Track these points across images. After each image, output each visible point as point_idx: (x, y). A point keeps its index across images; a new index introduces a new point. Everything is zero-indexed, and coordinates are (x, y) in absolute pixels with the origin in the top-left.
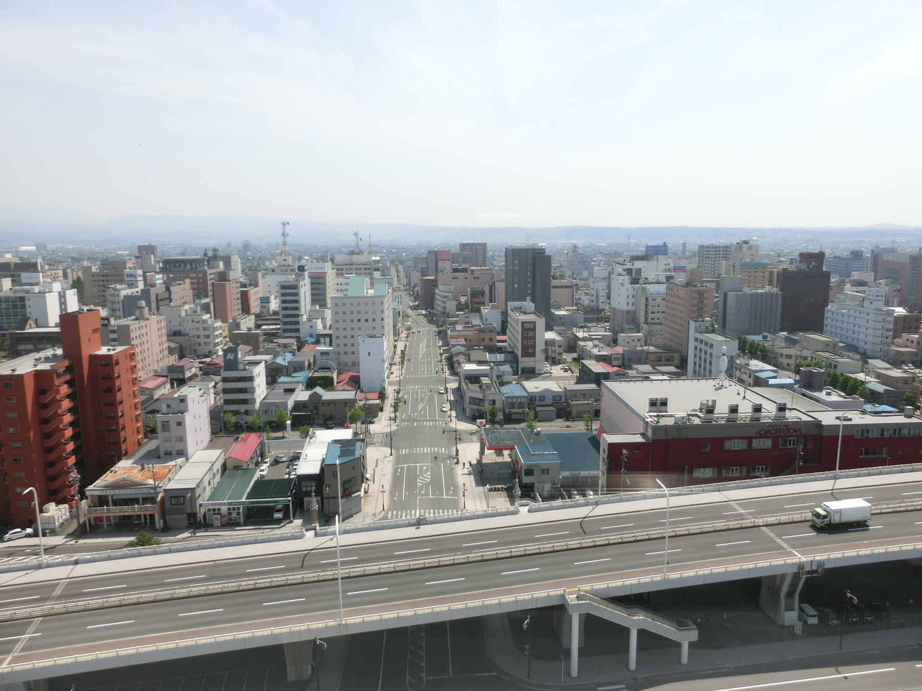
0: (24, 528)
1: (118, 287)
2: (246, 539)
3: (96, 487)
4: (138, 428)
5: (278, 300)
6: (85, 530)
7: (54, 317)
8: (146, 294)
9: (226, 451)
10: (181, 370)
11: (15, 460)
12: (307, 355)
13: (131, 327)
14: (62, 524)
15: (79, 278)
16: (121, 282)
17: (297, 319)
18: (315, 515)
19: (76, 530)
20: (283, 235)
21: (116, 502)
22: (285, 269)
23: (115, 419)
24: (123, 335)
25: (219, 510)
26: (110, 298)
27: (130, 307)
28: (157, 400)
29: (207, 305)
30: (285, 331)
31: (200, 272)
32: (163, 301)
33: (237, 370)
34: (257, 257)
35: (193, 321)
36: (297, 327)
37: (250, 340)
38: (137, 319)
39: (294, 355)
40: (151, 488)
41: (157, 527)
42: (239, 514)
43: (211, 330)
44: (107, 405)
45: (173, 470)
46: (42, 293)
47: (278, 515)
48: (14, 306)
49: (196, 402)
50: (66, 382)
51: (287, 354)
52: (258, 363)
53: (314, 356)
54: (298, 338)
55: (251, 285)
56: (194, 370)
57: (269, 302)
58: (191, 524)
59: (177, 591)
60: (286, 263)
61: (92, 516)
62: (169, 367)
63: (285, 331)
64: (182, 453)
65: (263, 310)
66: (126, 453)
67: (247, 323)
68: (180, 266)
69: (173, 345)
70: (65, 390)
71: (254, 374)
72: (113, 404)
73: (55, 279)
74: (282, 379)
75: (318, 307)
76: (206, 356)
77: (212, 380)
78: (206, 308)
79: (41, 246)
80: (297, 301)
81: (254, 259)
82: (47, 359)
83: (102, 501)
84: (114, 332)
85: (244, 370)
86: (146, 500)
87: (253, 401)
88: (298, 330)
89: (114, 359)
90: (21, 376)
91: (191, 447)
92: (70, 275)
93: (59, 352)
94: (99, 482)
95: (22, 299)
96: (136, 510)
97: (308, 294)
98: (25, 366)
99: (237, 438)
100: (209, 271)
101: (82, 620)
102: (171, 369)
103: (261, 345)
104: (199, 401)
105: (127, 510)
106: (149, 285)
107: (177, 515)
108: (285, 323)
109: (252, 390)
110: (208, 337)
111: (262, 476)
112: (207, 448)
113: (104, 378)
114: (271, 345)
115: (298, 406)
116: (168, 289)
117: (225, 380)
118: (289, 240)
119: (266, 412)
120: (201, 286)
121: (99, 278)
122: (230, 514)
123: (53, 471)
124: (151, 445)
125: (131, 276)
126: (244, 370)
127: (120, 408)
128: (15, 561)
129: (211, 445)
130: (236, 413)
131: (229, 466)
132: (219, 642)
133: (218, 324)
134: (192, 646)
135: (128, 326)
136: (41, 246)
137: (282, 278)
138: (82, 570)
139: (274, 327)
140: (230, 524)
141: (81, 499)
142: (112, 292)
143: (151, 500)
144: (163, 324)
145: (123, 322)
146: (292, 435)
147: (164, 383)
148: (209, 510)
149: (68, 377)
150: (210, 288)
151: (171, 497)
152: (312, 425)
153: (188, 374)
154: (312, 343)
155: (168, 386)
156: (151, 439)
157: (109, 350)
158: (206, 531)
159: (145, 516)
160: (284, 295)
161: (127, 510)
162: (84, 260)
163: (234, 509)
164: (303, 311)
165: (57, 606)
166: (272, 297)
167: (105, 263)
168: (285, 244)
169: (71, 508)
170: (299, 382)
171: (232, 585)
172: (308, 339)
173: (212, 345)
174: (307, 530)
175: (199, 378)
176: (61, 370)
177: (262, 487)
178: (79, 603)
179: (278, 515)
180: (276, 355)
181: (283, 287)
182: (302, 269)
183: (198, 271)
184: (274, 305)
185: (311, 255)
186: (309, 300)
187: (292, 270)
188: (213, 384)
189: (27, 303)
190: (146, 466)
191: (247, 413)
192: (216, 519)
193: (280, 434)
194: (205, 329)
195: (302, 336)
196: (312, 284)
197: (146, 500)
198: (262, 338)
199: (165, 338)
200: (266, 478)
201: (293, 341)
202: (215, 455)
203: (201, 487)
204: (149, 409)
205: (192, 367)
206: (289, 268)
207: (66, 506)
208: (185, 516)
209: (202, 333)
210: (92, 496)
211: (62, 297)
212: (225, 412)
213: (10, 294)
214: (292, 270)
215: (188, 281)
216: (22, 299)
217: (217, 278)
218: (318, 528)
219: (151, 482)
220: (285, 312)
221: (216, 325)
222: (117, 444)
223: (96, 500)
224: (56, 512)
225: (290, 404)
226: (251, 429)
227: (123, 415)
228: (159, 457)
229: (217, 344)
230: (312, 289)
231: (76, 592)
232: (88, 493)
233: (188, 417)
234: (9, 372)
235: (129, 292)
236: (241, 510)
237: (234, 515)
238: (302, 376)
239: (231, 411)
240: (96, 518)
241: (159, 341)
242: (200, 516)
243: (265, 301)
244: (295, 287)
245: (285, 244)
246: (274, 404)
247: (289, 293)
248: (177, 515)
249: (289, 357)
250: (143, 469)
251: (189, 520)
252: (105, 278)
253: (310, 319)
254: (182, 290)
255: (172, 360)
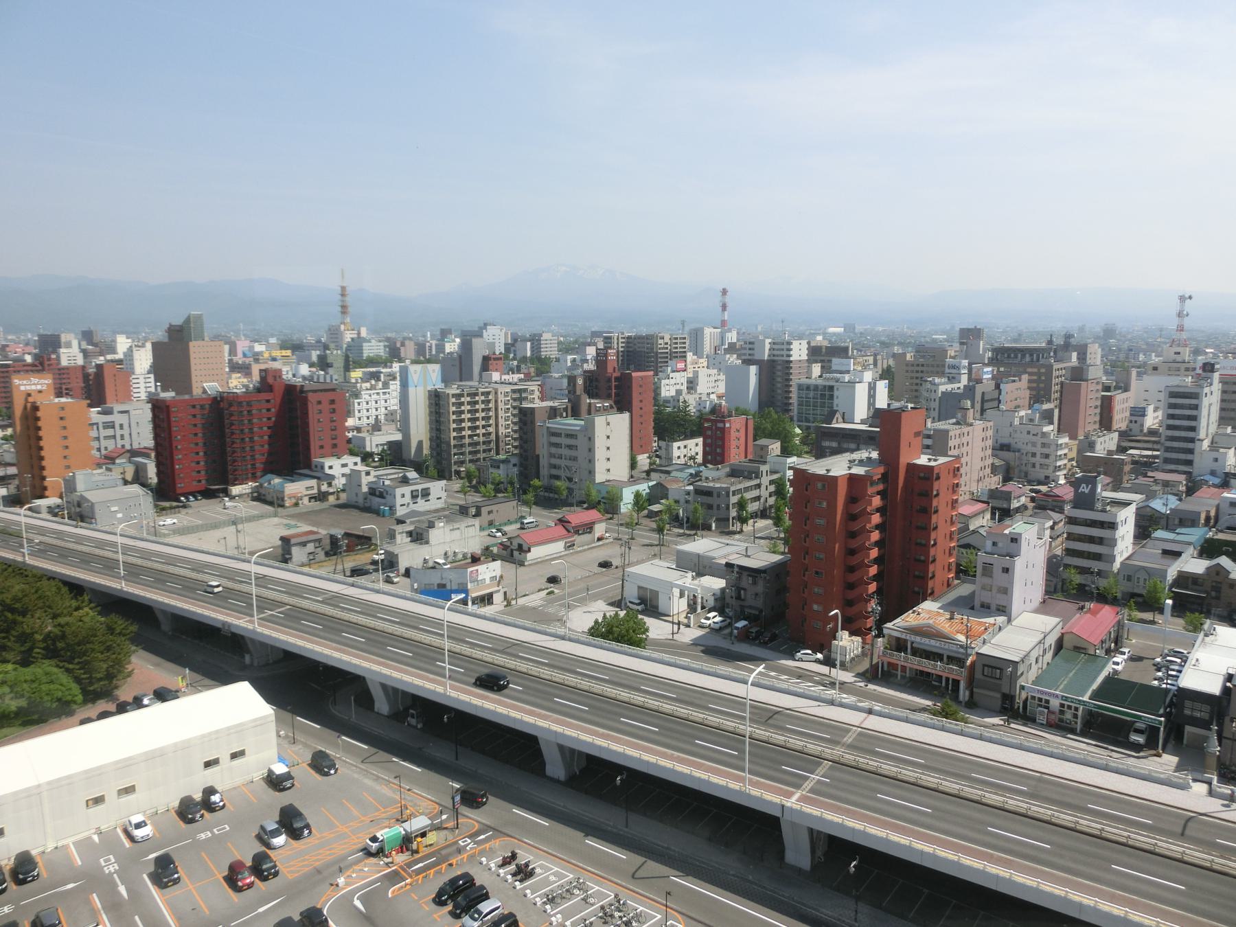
0: (815, 652)
1: (937, 380)
2: (1067, 753)
3: (895, 626)
4: (950, 564)
5: (1160, 414)
6: (879, 674)
7: (861, 411)
8: (969, 391)
9: (1065, 621)
10: (1007, 497)
11: (817, 573)
12: (1206, 501)
13: (951, 433)
14: (853, 659)
15: (889, 367)
16: (941, 374)
17: (1190, 445)
18: (1213, 762)
19: (866, 671)
20: (1180, 315)
21: (917, 652)
22: (1175, 366)
23: (926, 547)
24: (937, 443)
25: (1047, 702)
26: (925, 394)
27: (951, 407)
28: (974, 532)
29: (1051, 412)
30: (1166, 461)
31: (1043, 366)
32: (989, 404)
33: (1092, 509)
34: (1125, 346)
35: (1029, 433)
36: (1189, 457)
37: (1110, 467)
38: (958, 423)
39: (1180, 500)
40: (961, 646)
41: (961, 698)
42: (1075, 716)
43: (1053, 447)
44: (918, 528)
45: (990, 630)
46: (852, 383)
47: (1140, 739)
48: (823, 396)
49: (1032, 545)
50: (878, 493)
51: (1170, 497)
52: (1126, 504)
53: (1218, 507)
54: (1189, 474)
55: (1117, 388)
56: (1023, 499)
57: (1144, 415)
58: (1005, 709)
59: (987, 795)
60: (1179, 358)
61: (886, 660)
62: (991, 490)
63: (1166, 461)
64: (1003, 610)
65: (1133, 426)
66: (932, 593)
67: (1106, 444)
68: (1016, 357)
69: (998, 462)
70: (877, 501)
71: (1118, 520)
72: (926, 529)
73: (865, 367)
74: (1159, 534)
75: (1229, 430)
76: (1040, 483)
77: (1050, 518)
78: (1047, 417)
79: (849, 328)
80: (1194, 418)
81: (1120, 350)
82: (861, 463)
83: (899, 645)
84: (929, 437)
85: (1104, 511)
86: (951, 659)
87: (1112, 558)
88: (1189, 463)
89: (936, 472)
90: (835, 478)
91: (1016, 605)
92: (879, 363)
93: (875, 455)
94: (898, 621)
95: (831, 388)
96: (936, 668)
97: (1215, 410)
98: (838, 466)
99: (1082, 608)
100: (1055, 367)
101: (873, 784)
102: (993, 494)
103: (1125, 478)
104: (1035, 544)
105: (927, 666)
106: (975, 380)
107: (982, 690)
108: (1168, 449)
109: (1113, 543)
110: (1047, 456)
111: (1115, 672)
112: (1037, 611)
113: (920, 495)
114: (1141, 480)
115: (1184, 579)
116: (998, 387)
117: (1072, 521)
118: (1187, 322)
119: (1129, 578)
120: (1042, 385)
121: (915, 367)
122: (1062, 712)
123: (851, 595)
124: (964, 589)
125: (954, 367)
126: (1104, 511)
127: (933, 535)
128: (805, 686)
129: (1044, 608)
130: (1083, 571)
131: (1066, 643)
132: (962, 865)
133: (1064, 440)
134: (1004, 879)
135: (947, 431)
136: (849, 328)
137: (1174, 381)
138: (874, 723)
139: (1149, 453)
140: (1060, 726)
141: (878, 636)
142: (929, 386)
143: (960, 662)
144: (990, 433)
145: (941, 425)
146: (1170, 624)
147: (983, 512)
148: (1033, 698)
149: (881, 487)
150: (1056, 388)
151: (984, 665)
152: (1208, 614)
153: (1015, 504)
154: (1215, 486)
155: (988, 516)
156: (963, 582)
157: (930, 460)
158: (1025, 725)
159: (947, 679)
160: (1172, 406)
161: (927, 666)
162: (894, 345)
163: (1069, 707)
164: (1202, 435)
165: (847, 756)
166: (1150, 409)
167: (921, 350)
168: (1181, 329)
169: (864, 642)
170: (1189, 544)
171: (1066, 818)
172: (1207, 477)
173: (1051, 469)
174: (1195, 780)
175: (1030, 512)
176: (876, 478)
177: (1114, 688)
178: (871, 763)
179: (1140, 739)
180: (1151, 495)
181: (1173, 395)
182: (1209, 368)
183: (1039, 366)
184: (1152, 419)
185: (1217, 347)
186: (1215, 416)
187: (1187, 369)
188: (1051, 523)
189: (836, 393)
190: (957, 616)
191: (1100, 573)
192: (1041, 713)
193: (1148, 616)
194: (1044, 445)
195: (1194, 474)
196: (1224, 392)
197: (951, 659)
198: (1127, 468)
199: (989, 452)
200: (1122, 677)
201: (1182, 478)
202: (1049, 624)
203: (1027, 663)
204: (962, 542)
205: (1021, 497)
206: (1183, 366)
207: (859, 639)
208: (998, 696)
209: (1039, 450)
210: (890, 636)
211: (872, 388)
212: (1067, 566)
213: (820, 382)
214: (1187, 369)
215: (1025, 377)
216: (831, 388)
217: (1069, 376)
218: (1215, 782)
219: (962, 638)
220: (1170, 433)
221: (1060, 442)
222: (923, 578)
223: (894, 643)
224: (847, 643)
225: (1172, 574)
226: (1103, 598)
227: (935, 544)
228: (972, 608)
229: (1059, 468)
230: (1223, 401)
231: (635, 685)
232: (885, 631)
233: (1019, 563)
234: (823, 472)
235: (949, 387)
236: (1080, 713)
237: (1068, 715)
238: (1196, 534)
239: (1076, 567)
240: (889, 663)
241: (982, 454)
242: (1019, 701)
243: (1138, 413)
244: (1195, 396)
245: (1181, 329)
246: (1144, 568)
247: (1183, 407)
248: (982, 690)
249: (1173, 502)
250: (952, 618)
251: (1003, 703)
252: (920, 369)
253: (1214, 446)
254: (1017, 390)
255: (994, 482)
